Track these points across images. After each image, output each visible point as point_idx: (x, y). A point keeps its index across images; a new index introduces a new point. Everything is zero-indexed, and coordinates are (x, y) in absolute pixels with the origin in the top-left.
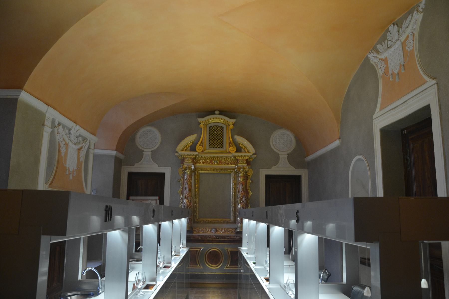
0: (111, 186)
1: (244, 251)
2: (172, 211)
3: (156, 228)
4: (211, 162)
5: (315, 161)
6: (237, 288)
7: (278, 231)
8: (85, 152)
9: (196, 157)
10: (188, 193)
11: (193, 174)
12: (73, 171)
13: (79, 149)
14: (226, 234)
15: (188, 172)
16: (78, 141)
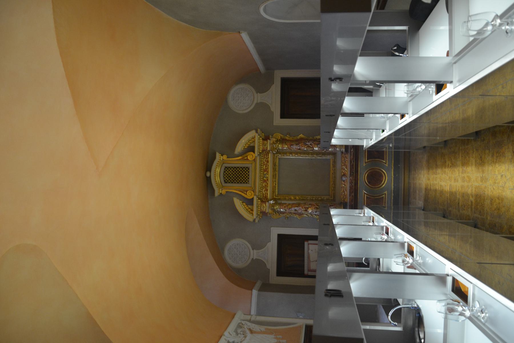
0: (292, 295)
1: (367, 143)
2: (324, 224)
3: (344, 242)
4: (265, 181)
5: (264, 61)
6: (410, 152)
7: (349, 104)
8: (254, 325)
9: (259, 199)
10: (301, 208)
11: (279, 202)
12: (276, 338)
13: (252, 332)
14: (348, 164)
15: (277, 207)
16: (242, 333)
